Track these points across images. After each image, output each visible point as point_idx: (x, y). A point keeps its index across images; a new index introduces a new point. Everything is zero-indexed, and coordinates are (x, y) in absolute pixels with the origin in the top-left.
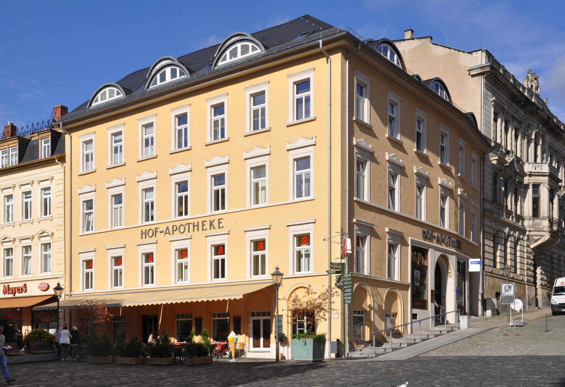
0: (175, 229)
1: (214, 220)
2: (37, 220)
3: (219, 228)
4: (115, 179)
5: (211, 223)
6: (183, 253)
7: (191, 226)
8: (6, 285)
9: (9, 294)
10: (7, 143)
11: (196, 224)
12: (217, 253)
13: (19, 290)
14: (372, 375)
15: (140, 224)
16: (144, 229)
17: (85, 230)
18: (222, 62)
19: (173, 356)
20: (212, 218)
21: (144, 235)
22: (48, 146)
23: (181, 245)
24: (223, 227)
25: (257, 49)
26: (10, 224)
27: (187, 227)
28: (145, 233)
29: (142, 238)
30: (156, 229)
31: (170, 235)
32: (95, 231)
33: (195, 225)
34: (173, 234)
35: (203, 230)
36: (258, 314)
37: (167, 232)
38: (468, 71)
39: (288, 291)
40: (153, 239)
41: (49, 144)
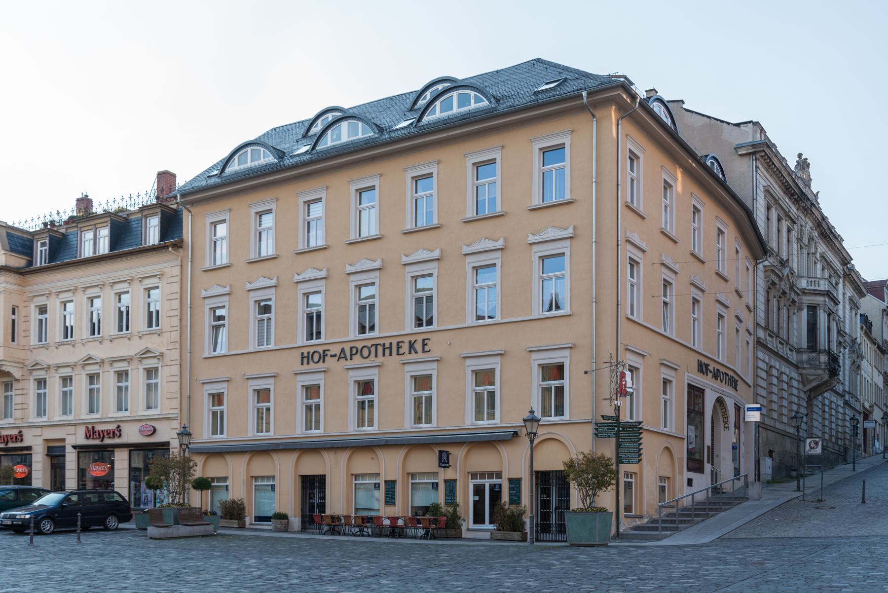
0: (355, 352)
1: (416, 340)
2: (81, 341)
3: (424, 351)
4: (262, 278)
5: (411, 346)
6: (422, 382)
7: (380, 349)
8: (90, 427)
9: (93, 438)
10: (92, 223)
11: (387, 345)
12: (364, 393)
13: (12, 438)
15: (299, 344)
16: (305, 351)
18: (428, 117)
20: (413, 339)
21: (305, 360)
22: (45, 250)
23: (364, 375)
24: (429, 351)
25: (484, 101)
26: (97, 339)
27: (373, 350)
28: (308, 357)
29: (302, 364)
30: (324, 351)
32: (325, 340)
33: (386, 347)
34: (351, 359)
35: (398, 354)
36: (482, 475)
37: (342, 355)
40: (321, 366)
41: (47, 248)
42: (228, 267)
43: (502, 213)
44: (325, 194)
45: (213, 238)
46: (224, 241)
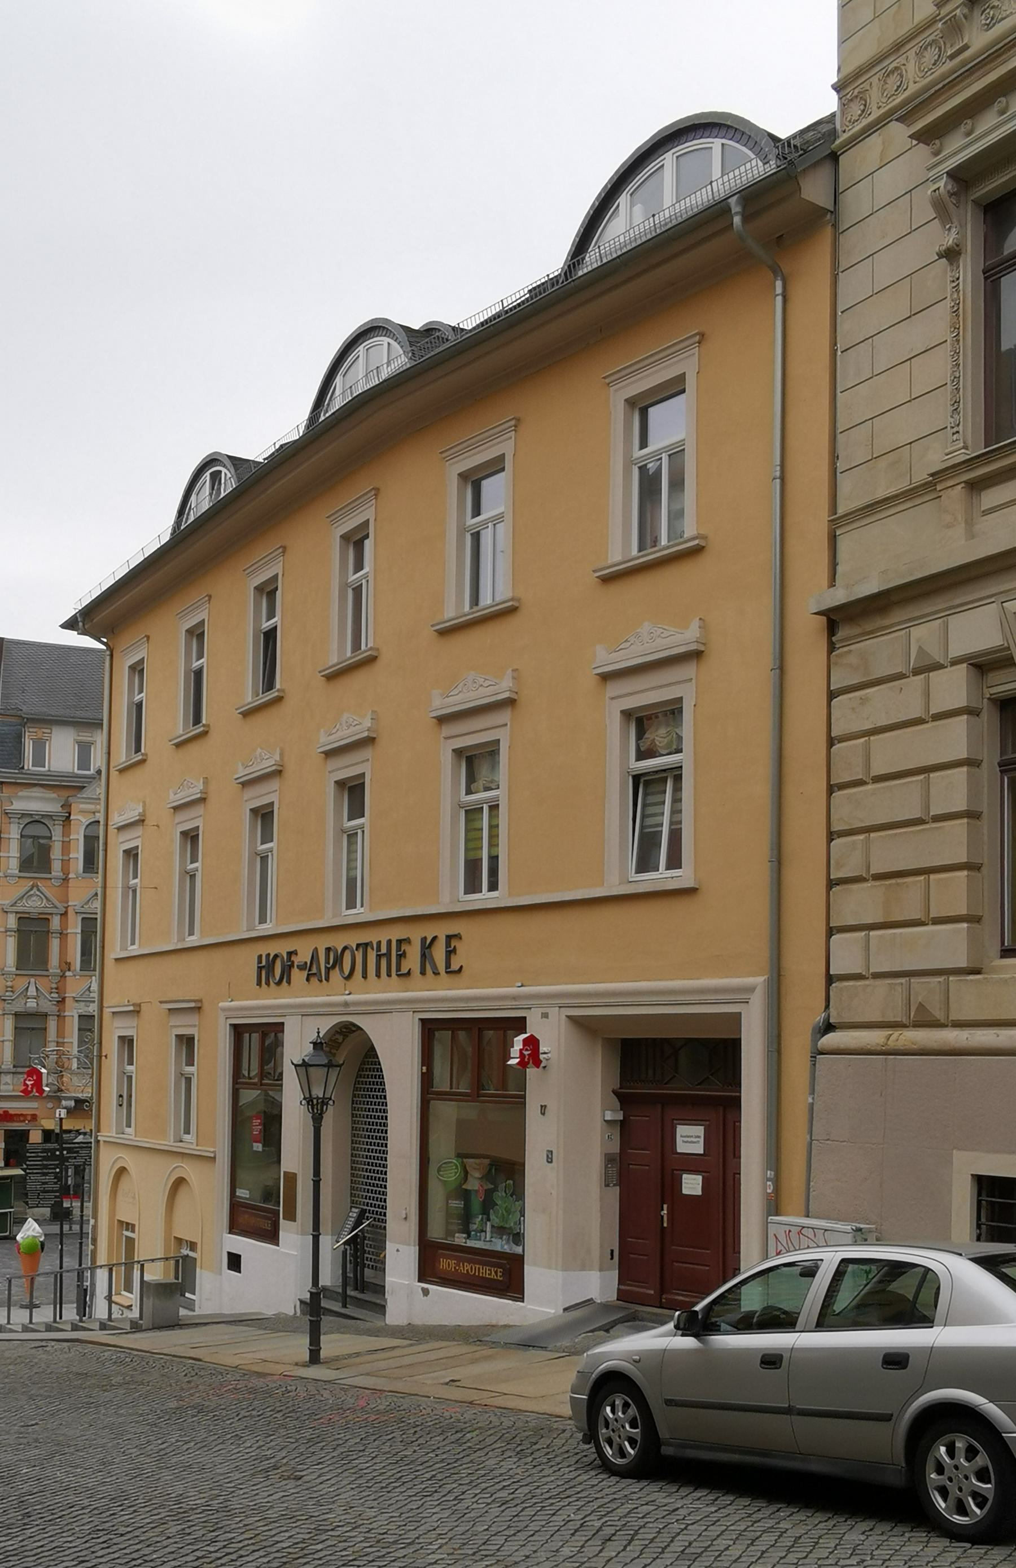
14: (862, 1226)
19: (665, 1299)
31: (321, 981)
32: (510, 895)
34: (327, 980)
38: (371, 660)
39: (166, 1185)
46: (500, 527)
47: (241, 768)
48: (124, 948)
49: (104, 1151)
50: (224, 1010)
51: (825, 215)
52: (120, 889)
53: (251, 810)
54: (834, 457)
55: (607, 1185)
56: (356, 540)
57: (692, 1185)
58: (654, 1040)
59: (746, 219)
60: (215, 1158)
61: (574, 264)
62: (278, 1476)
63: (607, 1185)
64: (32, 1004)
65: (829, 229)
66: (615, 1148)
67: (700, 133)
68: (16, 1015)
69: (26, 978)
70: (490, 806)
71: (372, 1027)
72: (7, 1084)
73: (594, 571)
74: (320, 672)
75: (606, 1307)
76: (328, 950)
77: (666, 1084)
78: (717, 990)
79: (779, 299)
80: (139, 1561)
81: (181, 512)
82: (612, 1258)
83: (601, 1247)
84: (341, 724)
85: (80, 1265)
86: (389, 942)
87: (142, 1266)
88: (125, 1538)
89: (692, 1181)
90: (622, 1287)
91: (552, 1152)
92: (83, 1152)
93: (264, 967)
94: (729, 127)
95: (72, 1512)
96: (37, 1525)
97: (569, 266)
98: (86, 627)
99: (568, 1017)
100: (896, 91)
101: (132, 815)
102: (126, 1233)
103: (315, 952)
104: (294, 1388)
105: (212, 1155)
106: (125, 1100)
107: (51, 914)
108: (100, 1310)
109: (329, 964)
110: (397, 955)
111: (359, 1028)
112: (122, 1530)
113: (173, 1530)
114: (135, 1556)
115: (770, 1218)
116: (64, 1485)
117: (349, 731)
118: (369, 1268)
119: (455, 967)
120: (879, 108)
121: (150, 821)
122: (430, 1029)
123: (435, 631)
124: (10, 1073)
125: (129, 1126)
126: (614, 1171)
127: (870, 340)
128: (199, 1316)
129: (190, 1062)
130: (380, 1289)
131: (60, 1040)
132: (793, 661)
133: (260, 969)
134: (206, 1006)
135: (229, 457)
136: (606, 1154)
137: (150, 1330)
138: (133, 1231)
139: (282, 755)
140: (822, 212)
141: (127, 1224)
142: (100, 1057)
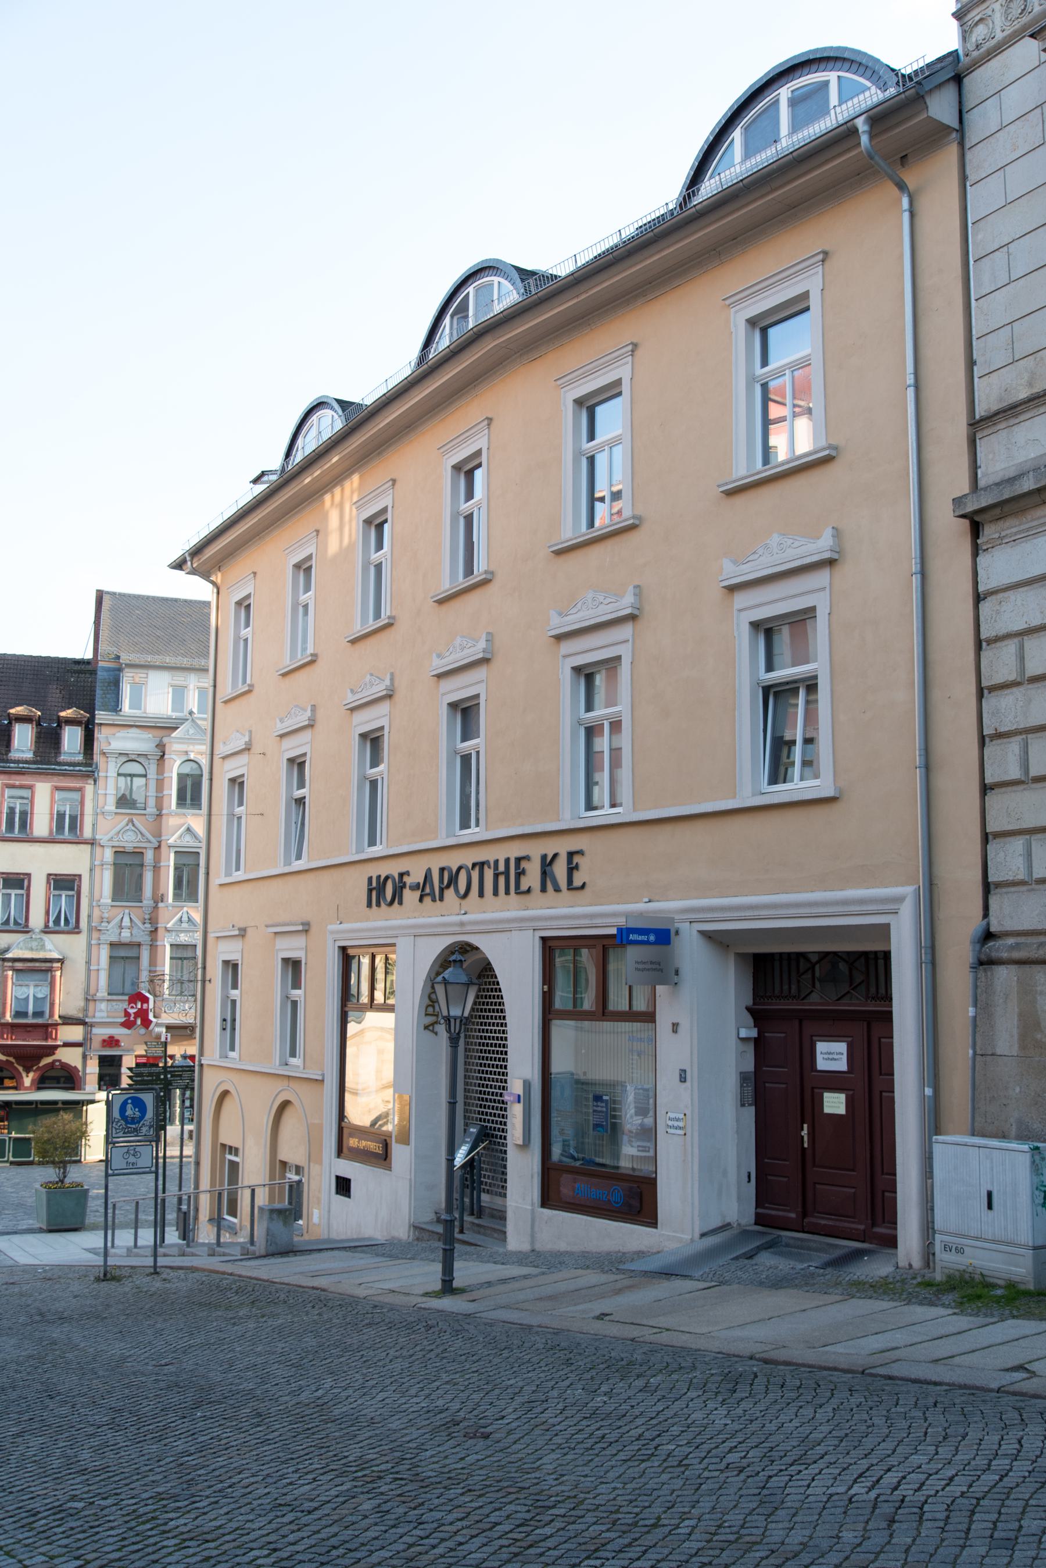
7: (489, 874)
17: (293, 857)
25: (468, 293)
31: (434, 900)
32: (635, 810)
34: (441, 899)
42: (827, 460)
43: (631, 522)
44: (629, 366)
45: (759, 371)
46: (618, 451)
47: (350, 694)
48: (228, 874)
49: (207, 1074)
50: (332, 932)
51: (949, 134)
52: (225, 817)
53: (360, 735)
54: (971, 363)
55: (743, 1105)
56: (466, 470)
57: (835, 1103)
58: (789, 954)
59: (872, 136)
60: (323, 1081)
61: (689, 194)
62: (462, 1433)
63: (743, 1105)
64: (126, 935)
65: (953, 149)
66: (750, 1066)
67: (814, 67)
68: (112, 945)
69: (120, 909)
70: (610, 723)
71: (490, 947)
72: (101, 1011)
73: (719, 486)
74: (432, 598)
75: (745, 1234)
76: (442, 870)
77: (803, 999)
78: (862, 901)
79: (906, 216)
80: (341, 1551)
81: (288, 454)
82: (749, 1181)
83: (739, 1167)
84: (454, 647)
85: (180, 1190)
86: (507, 861)
87: (253, 1191)
88: (315, 1517)
89: (834, 1100)
90: (760, 1210)
91: (685, 1071)
92: (186, 1075)
93: (374, 888)
94: (844, 59)
95: (243, 1479)
96: (207, 1497)
97: (684, 198)
98: (194, 566)
99: (699, 931)
100: (1020, 14)
101: (239, 744)
102: (229, 1157)
103: (429, 871)
104: (435, 1322)
105: (320, 1078)
106: (229, 1024)
107: (146, 848)
108: (205, 1234)
109: (443, 883)
110: (516, 873)
111: (477, 948)
112: (308, 1505)
113: (367, 1506)
114: (334, 1541)
115: (935, 1137)
116: (223, 1442)
117: (461, 654)
118: (484, 1192)
119: (577, 883)
120: (1003, 31)
121: (256, 748)
122: (549, 947)
123: (552, 552)
124: (104, 1000)
125: (232, 1049)
126: (750, 1090)
127: (1006, 248)
128: (309, 1242)
129: (296, 985)
130: (500, 1216)
131: (153, 969)
132: (935, 566)
133: (370, 891)
134: (314, 930)
135: (337, 400)
136: (741, 1073)
137: (265, 1256)
138: (236, 1155)
139: (392, 680)
140: (948, 129)
141: (231, 1147)
142: (204, 981)
